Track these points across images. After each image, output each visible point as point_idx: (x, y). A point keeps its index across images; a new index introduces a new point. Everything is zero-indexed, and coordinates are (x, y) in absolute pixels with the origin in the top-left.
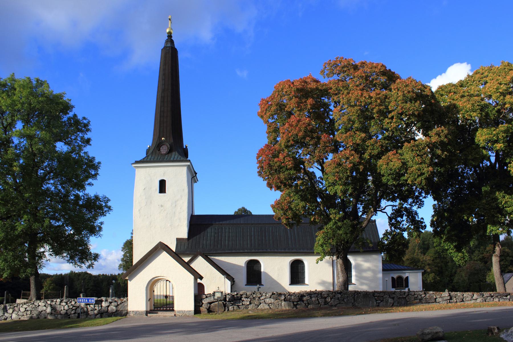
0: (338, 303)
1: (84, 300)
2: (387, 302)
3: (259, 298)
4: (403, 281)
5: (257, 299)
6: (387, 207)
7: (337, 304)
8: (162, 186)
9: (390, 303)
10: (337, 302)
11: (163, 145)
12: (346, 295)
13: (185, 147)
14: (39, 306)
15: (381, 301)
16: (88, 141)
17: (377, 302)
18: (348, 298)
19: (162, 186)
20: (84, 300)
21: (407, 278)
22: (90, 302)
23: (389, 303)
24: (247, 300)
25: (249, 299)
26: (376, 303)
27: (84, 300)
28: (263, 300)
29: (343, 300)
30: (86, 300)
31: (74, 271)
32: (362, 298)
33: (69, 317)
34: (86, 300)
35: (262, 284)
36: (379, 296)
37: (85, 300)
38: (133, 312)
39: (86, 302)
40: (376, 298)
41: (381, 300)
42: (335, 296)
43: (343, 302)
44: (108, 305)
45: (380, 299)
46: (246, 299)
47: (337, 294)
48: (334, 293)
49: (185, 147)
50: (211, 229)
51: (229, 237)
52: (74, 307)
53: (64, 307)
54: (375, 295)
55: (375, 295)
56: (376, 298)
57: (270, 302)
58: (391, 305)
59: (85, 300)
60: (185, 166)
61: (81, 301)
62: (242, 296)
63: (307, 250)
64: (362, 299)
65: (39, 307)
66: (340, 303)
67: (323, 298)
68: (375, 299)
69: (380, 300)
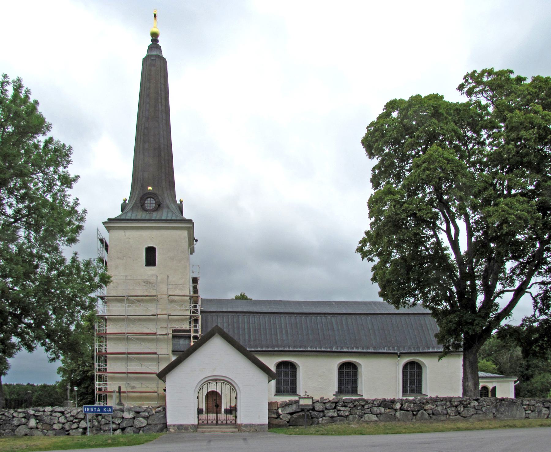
0: (474, 413)
1: (94, 410)
2: (540, 412)
3: (363, 406)
4: (488, 392)
5: (359, 408)
6: (529, 294)
7: (473, 415)
8: (151, 253)
9: (545, 414)
10: (473, 411)
11: (153, 198)
12: (484, 403)
13: (178, 202)
14: (14, 417)
15: (532, 411)
16: (67, 181)
17: (527, 412)
18: (488, 407)
19: (151, 253)
20: (95, 408)
21: (494, 389)
22: (105, 412)
23: (542, 415)
24: (345, 410)
25: (348, 409)
26: (526, 414)
27: (94, 410)
28: (368, 409)
29: (481, 410)
30: (99, 409)
31: (8, 372)
32: (506, 406)
33: (67, 433)
34: (99, 409)
35: (298, 393)
36: (529, 405)
37: (97, 410)
38: (174, 425)
39: (98, 412)
40: (525, 407)
41: (532, 409)
42: (469, 404)
43: (480, 412)
44: (133, 416)
45: (531, 409)
46: (344, 408)
47: (473, 402)
48: (468, 400)
49: (178, 202)
50: (222, 318)
51: (249, 329)
52: (76, 418)
53: (59, 419)
54: (524, 403)
55: (524, 403)
56: (525, 407)
57: (378, 412)
58: (546, 416)
59: (97, 410)
60: (185, 230)
61: (90, 410)
62: (338, 404)
63: (363, 349)
64: (507, 408)
65: (14, 419)
66: (477, 413)
67: (453, 406)
68: (524, 408)
69: (530, 410)
